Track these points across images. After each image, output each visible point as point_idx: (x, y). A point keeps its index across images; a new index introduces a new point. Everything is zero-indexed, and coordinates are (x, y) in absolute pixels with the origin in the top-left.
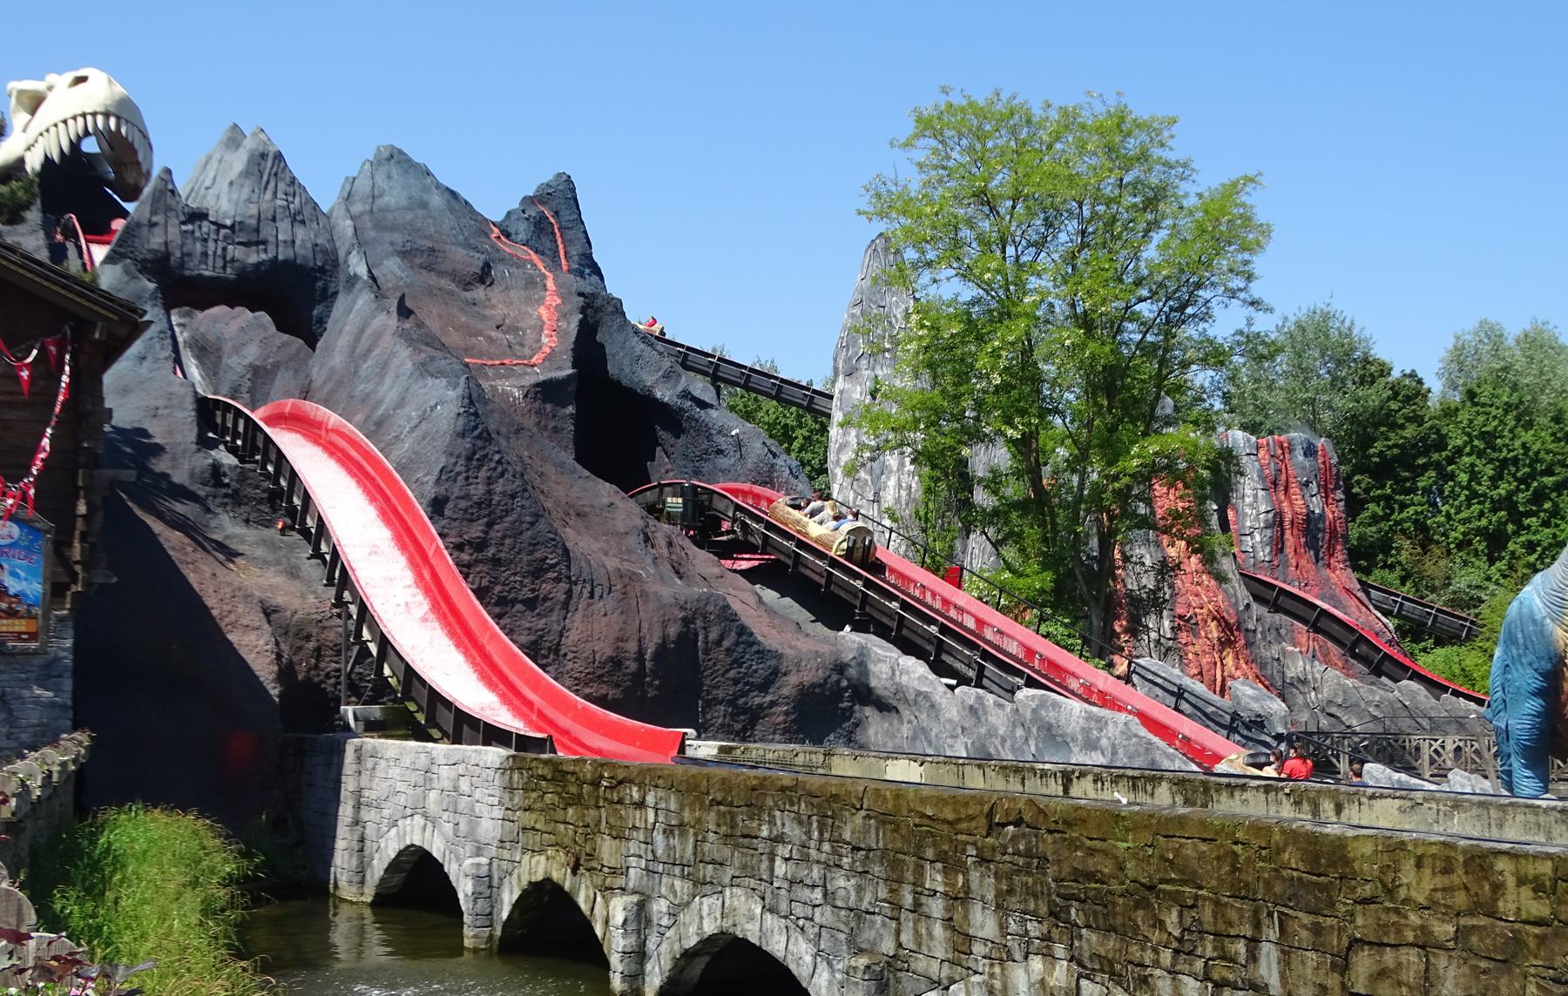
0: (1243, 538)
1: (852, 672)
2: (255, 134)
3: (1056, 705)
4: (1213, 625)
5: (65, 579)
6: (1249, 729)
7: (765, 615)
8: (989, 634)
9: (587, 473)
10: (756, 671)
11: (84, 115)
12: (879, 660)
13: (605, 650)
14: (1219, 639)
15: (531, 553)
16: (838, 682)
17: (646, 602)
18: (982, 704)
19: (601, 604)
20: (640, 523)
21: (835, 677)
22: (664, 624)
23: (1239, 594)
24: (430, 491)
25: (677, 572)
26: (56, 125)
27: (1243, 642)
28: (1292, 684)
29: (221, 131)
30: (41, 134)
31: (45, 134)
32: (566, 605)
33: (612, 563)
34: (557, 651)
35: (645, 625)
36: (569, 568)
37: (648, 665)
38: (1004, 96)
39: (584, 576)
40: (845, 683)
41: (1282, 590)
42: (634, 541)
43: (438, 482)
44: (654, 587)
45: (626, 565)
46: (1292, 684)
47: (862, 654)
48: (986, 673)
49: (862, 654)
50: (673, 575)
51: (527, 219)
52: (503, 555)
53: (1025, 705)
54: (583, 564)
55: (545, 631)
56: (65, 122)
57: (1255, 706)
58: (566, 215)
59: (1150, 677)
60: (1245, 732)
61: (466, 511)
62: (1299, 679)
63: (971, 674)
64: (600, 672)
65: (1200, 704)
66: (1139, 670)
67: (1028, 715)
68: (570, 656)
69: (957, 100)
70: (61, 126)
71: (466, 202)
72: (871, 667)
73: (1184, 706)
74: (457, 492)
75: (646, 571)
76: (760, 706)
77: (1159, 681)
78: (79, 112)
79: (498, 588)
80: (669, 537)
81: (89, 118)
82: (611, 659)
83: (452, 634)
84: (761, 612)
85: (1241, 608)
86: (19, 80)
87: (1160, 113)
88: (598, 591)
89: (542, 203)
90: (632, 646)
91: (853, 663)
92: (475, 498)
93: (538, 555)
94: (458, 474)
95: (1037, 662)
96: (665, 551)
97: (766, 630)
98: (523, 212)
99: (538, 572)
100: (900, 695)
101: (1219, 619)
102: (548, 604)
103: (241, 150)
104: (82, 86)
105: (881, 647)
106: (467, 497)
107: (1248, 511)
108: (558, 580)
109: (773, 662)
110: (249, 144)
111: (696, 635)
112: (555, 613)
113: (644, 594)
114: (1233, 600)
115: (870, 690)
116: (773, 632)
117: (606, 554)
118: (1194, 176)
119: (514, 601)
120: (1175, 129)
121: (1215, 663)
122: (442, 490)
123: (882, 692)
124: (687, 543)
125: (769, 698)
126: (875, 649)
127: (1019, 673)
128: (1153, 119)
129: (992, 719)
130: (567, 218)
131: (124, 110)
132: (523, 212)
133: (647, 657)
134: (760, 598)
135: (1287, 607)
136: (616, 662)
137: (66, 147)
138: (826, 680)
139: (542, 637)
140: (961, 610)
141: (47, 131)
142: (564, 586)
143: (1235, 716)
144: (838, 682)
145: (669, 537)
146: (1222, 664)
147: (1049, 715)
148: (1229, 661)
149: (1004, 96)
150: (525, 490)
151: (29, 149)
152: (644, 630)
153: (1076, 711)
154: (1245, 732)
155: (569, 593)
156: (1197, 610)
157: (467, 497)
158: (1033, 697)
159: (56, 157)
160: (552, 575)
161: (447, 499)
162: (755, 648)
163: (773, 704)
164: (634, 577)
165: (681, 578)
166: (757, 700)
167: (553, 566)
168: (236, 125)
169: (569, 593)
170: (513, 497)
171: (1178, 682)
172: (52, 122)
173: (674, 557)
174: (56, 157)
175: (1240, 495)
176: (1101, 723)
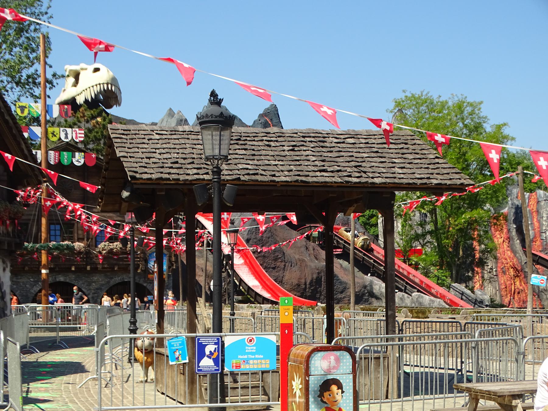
0: (542, 234)
1: (368, 288)
2: (178, 113)
3: (422, 297)
4: (512, 270)
5: (170, 265)
6: (480, 304)
7: (343, 271)
8: (411, 277)
9: (288, 228)
10: (339, 288)
11: (100, 84)
12: (376, 285)
13: (295, 282)
14: (514, 275)
15: (274, 254)
16: (364, 291)
17: (307, 268)
18: (404, 297)
19: (294, 268)
20: (305, 243)
21: (363, 290)
22: (312, 274)
23: (522, 259)
24: (246, 237)
25: (316, 258)
26: (89, 88)
27: (523, 276)
28: (542, 291)
29: (165, 111)
30: (84, 91)
31: (85, 91)
32: (284, 269)
33: (297, 257)
34: (282, 282)
35: (307, 275)
36: (285, 258)
37: (308, 286)
38: (424, 94)
39: (289, 260)
40: (366, 291)
41: (540, 257)
42: (303, 249)
43: (248, 234)
44: (309, 263)
45: (301, 257)
46: (542, 291)
47: (371, 283)
48: (407, 288)
49: (371, 283)
50: (314, 259)
51: (261, 123)
52: (266, 255)
53: (414, 297)
54: (289, 257)
55: (278, 276)
56: (93, 86)
57: (480, 297)
58: (275, 120)
59: (455, 289)
60: (479, 305)
61: (256, 242)
62: (544, 290)
63: (403, 288)
64: (294, 288)
65: (468, 297)
66: (452, 287)
67: (415, 300)
68: (285, 283)
69: (409, 95)
70: (91, 88)
71: (240, 119)
72: (374, 286)
73: (464, 297)
74: (253, 237)
75: (307, 259)
76: (341, 298)
77: (458, 290)
78: (98, 83)
79: (265, 264)
80: (313, 247)
81: (102, 85)
82: (297, 284)
83: (255, 276)
84: (342, 270)
85: (523, 264)
86: (70, 65)
87: (478, 100)
88: (293, 265)
89: (266, 116)
90: (303, 281)
91: (369, 285)
92: (258, 239)
93: (276, 255)
94: (253, 232)
95: (424, 285)
96: (312, 252)
97: (343, 276)
98: (259, 120)
99: (276, 259)
100: (382, 295)
101: (514, 268)
102: (279, 268)
103: (174, 118)
104: (97, 73)
105: (377, 281)
106: (256, 238)
107: (544, 223)
108: (282, 262)
109: (345, 285)
110: (176, 116)
111: (321, 277)
112: (281, 271)
113: (306, 265)
114: (520, 261)
115: (373, 293)
116: (345, 276)
117: (295, 254)
118: (489, 122)
119: (269, 268)
120: (482, 106)
121: (512, 284)
122: (249, 237)
123: (377, 294)
124: (319, 249)
125: (343, 296)
126: (375, 281)
127: (416, 288)
128: (475, 102)
129: (406, 301)
130: (275, 121)
131: (114, 81)
132: (259, 120)
133: (308, 284)
134: (341, 266)
135: (542, 263)
136: (299, 285)
137: (93, 97)
138: (360, 291)
139: (277, 278)
140: (403, 269)
141: (86, 89)
142: (283, 263)
143: (476, 300)
144: (364, 291)
145: (313, 247)
146: (515, 284)
147: (421, 300)
148: (518, 283)
149: (424, 94)
150: (272, 236)
151: (78, 95)
152: (307, 276)
153: (427, 299)
154: (479, 305)
155: (285, 265)
156: (506, 265)
157: (256, 238)
158: (417, 295)
159: (90, 100)
160: (280, 260)
161: (250, 239)
162: (339, 281)
163: (344, 297)
164: (303, 261)
165: (317, 260)
166: (340, 296)
167: (280, 258)
168: (171, 109)
169: (285, 265)
170: (269, 238)
171: (462, 290)
172: (88, 87)
173: (315, 253)
174: (90, 100)
175: (541, 217)
176: (433, 302)
